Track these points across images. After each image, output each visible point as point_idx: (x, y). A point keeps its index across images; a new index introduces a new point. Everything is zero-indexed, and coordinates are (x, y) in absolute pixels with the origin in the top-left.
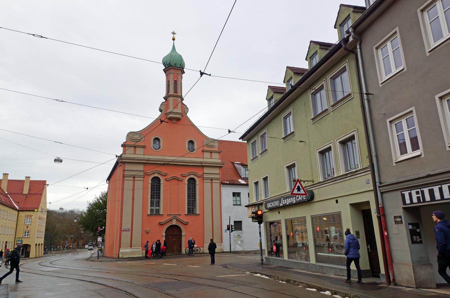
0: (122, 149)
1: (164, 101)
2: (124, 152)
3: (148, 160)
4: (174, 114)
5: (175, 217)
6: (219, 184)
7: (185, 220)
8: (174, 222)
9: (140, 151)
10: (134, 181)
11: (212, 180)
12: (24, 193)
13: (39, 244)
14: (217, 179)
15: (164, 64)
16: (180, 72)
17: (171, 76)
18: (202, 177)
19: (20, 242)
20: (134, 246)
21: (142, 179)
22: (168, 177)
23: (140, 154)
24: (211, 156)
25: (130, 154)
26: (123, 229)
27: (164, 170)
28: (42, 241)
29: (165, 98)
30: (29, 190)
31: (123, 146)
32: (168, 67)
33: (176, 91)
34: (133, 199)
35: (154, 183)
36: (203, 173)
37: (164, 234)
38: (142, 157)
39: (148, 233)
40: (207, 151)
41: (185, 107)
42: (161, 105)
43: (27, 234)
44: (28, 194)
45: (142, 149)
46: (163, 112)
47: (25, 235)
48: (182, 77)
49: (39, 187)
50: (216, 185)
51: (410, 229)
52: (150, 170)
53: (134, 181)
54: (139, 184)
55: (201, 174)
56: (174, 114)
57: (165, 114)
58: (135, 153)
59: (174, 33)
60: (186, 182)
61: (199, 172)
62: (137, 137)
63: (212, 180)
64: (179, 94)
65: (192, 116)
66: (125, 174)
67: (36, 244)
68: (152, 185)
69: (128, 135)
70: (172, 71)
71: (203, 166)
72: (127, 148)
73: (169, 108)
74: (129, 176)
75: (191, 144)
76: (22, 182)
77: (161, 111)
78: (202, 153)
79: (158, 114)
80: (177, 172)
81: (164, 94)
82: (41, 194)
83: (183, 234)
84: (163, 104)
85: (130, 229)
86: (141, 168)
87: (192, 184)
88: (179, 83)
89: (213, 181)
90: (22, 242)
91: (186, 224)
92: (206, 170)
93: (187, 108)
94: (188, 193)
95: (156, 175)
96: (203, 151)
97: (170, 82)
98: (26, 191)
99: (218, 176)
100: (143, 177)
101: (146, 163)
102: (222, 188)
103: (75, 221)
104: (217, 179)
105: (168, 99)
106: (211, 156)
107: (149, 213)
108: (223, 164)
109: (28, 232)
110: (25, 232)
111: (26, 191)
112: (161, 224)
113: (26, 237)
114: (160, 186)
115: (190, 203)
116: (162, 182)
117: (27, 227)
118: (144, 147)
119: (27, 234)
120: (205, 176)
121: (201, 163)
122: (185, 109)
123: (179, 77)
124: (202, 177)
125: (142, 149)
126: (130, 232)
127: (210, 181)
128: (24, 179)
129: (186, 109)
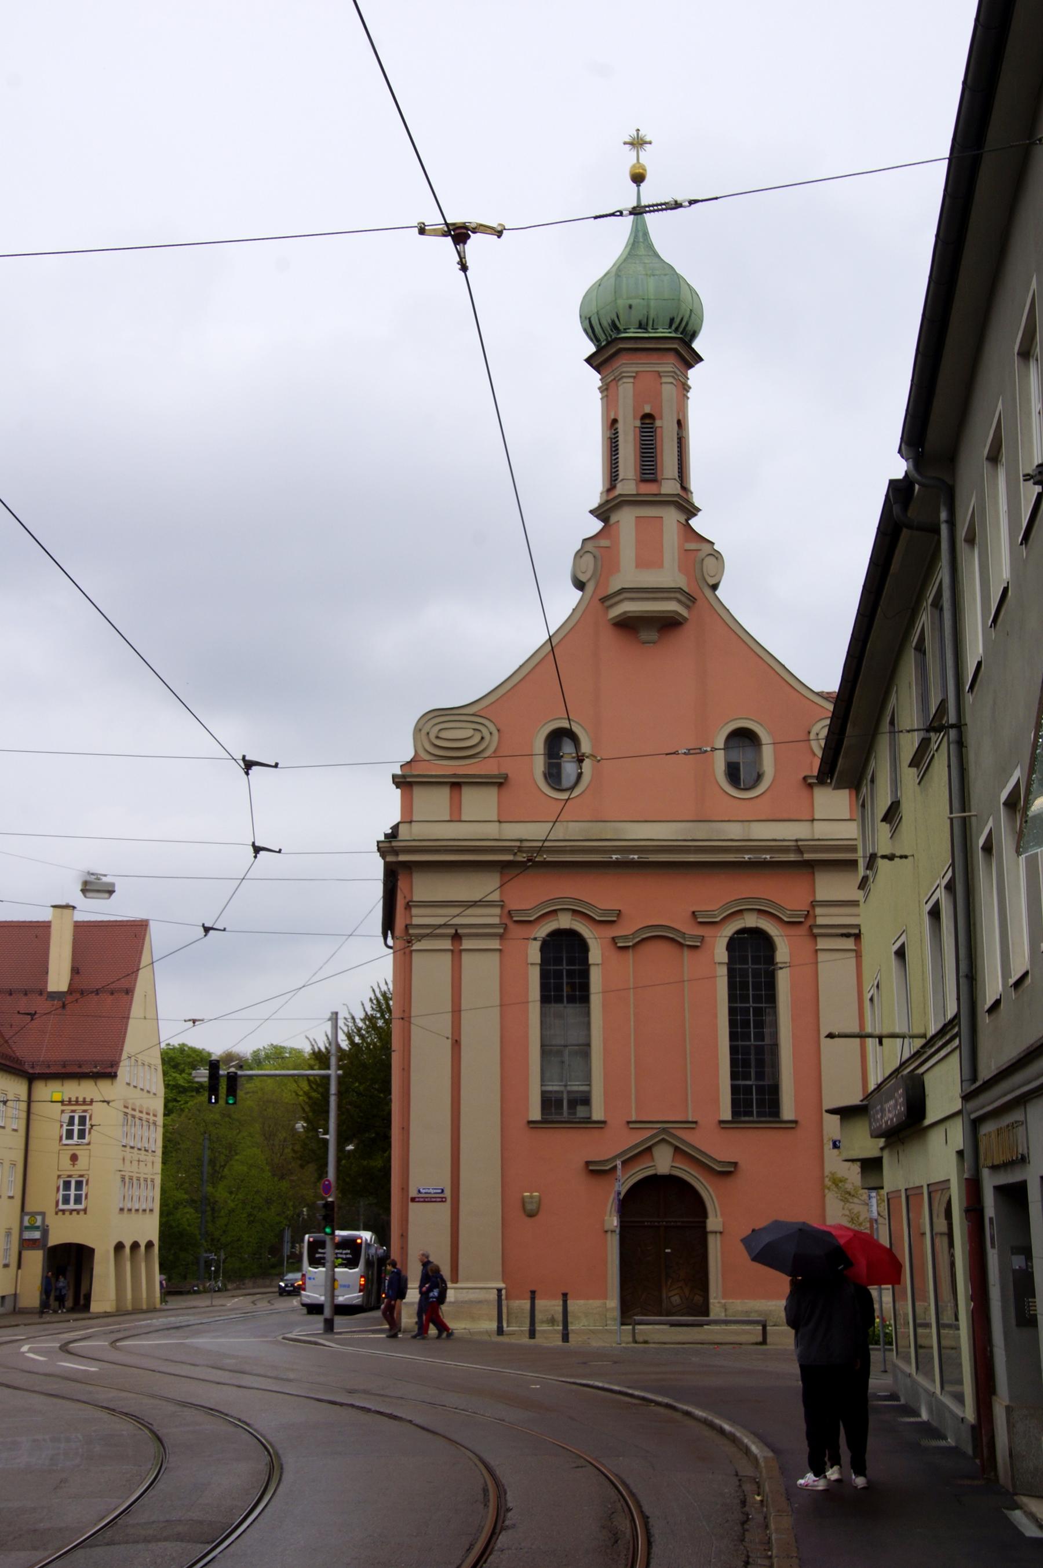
2: (407, 806)
5: (665, 1133)
8: (663, 1163)
9: (480, 804)
10: (457, 954)
12: (52, 987)
13: (135, 1246)
15: (591, 332)
16: (668, 364)
17: (626, 390)
18: (804, 923)
19: (37, 1235)
20: (467, 1280)
21: (495, 944)
23: (480, 819)
25: (438, 822)
27: (601, 894)
28: (148, 1229)
29: (603, 512)
30: (75, 971)
32: (609, 343)
33: (649, 471)
34: (456, 1043)
35: (558, 961)
36: (814, 904)
37: (614, 1222)
38: (491, 830)
39: (531, 1215)
41: (706, 547)
42: (579, 555)
43: (73, 1192)
44: (71, 990)
45: (492, 793)
46: (590, 588)
47: (66, 1200)
48: (686, 388)
49: (114, 955)
51: (1014, 1271)
52: (530, 894)
53: (457, 954)
54: (482, 969)
57: (603, 600)
58: (456, 818)
59: (638, 143)
60: (721, 954)
61: (788, 894)
62: (462, 733)
64: (669, 487)
66: (416, 921)
67: (119, 1247)
68: (544, 975)
69: (418, 730)
70: (627, 365)
71: (811, 867)
72: (418, 792)
73: (618, 570)
74: (432, 932)
76: (44, 928)
77: (580, 585)
78: (804, 792)
79: (565, 601)
80: (670, 904)
81: (594, 493)
82: (129, 992)
83: (713, 1223)
84: (589, 546)
85: (448, 1193)
86: (484, 887)
87: (756, 960)
88: (666, 426)
90: (45, 1232)
91: (727, 1172)
93: (717, 556)
94: (732, 1011)
95: (565, 922)
97: (620, 426)
98: (59, 979)
100: (501, 937)
103: (300, 1126)
105: (613, 519)
107: (536, 1114)
109: (79, 1185)
110: (67, 1185)
111: (59, 979)
112: (597, 1171)
113: (72, 1206)
114: (585, 974)
116: (595, 955)
117: (74, 1158)
118: (500, 783)
119: (73, 1192)
121: (799, 850)
122: (702, 558)
123: (668, 391)
124: (804, 923)
125: (491, 795)
126: (446, 1207)
128: (45, 915)
129: (710, 562)
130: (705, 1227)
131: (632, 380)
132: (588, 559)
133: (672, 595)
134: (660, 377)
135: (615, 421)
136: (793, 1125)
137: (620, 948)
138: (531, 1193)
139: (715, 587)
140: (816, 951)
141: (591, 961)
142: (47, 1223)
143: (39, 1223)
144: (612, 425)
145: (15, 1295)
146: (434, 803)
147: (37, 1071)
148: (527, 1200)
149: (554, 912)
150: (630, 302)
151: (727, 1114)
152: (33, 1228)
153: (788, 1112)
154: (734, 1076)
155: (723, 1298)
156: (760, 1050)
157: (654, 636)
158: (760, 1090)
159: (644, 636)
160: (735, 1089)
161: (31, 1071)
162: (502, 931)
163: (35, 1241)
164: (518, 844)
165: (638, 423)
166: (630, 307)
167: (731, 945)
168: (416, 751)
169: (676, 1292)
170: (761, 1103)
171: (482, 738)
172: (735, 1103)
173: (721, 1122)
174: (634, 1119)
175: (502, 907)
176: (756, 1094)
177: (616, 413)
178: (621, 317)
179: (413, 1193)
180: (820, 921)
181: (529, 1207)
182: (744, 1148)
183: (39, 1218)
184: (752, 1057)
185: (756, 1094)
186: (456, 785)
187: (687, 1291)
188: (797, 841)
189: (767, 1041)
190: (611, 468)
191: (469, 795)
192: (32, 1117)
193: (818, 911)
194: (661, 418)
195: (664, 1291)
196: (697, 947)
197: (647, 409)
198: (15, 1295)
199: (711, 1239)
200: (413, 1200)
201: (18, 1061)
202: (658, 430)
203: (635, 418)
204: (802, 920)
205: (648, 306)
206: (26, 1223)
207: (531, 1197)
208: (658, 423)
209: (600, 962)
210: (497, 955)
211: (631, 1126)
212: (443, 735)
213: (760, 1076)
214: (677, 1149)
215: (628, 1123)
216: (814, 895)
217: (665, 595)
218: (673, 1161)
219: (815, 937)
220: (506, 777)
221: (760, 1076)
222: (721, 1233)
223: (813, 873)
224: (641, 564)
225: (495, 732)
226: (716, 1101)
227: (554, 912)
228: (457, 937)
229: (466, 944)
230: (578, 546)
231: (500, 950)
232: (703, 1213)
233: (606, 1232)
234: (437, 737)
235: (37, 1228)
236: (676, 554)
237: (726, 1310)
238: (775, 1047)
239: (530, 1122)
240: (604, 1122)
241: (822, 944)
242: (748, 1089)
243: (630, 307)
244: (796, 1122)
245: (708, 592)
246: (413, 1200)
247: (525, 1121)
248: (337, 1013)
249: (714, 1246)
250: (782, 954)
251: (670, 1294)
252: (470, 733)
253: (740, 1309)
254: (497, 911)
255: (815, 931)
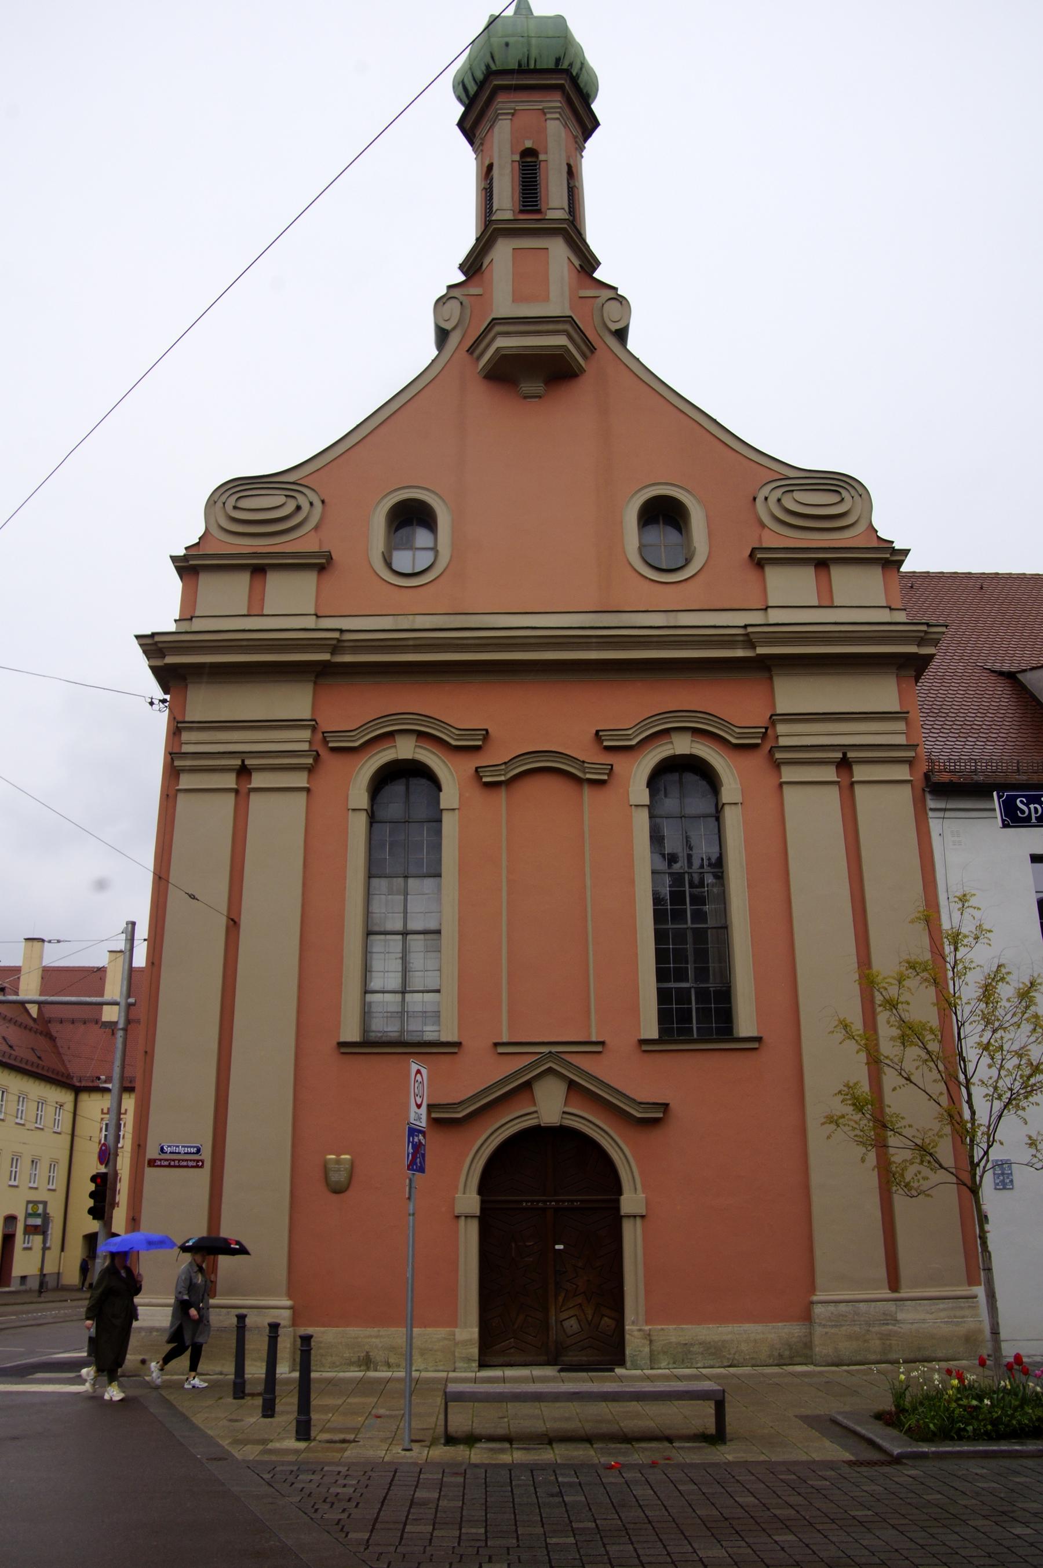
0: (174, 584)
1: (460, 278)
3: (336, 647)
4: (532, 334)
5: (552, 1061)
6: (906, 792)
7: (637, 1080)
8: (550, 1106)
10: (848, 790)
11: (844, 764)
14: (882, 755)
21: (300, 780)
22: (495, 756)
23: (291, 604)
24: (826, 590)
26: (152, 1152)
27: (459, 709)
31: (190, 566)
34: (233, 924)
36: (775, 719)
37: (470, 1201)
39: (338, 1190)
40: (791, 558)
41: (610, 294)
45: (308, 581)
50: (886, 803)
52: (352, 710)
53: (241, 795)
55: (762, 720)
56: (532, 334)
60: (640, 793)
61: (738, 706)
63: (844, 764)
65: (659, 343)
69: (212, 503)
71: (765, 667)
72: (207, 582)
75: (663, 536)
78: (752, 575)
81: (464, 236)
83: (631, 1201)
84: (455, 293)
85: (206, 1155)
86: (295, 702)
89: (860, 773)
91: (652, 1119)
92: (794, 695)
93: (621, 300)
96: (760, 561)
97: (495, 172)
99: (894, 734)
100: (310, 770)
101: (326, 666)
102: (935, 825)
104: (882, 755)
106: (826, 590)
108: (921, 642)
115: (680, 956)
118: (321, 565)
120: (788, 735)
121: (749, 642)
124: (760, 745)
126: (203, 1176)
127: (829, 773)
129: (613, 307)
130: (618, 1209)
131: (510, 117)
132: (454, 306)
133: (560, 327)
134: (545, 114)
135: (490, 167)
136: (755, 1045)
137: (488, 785)
138: (338, 1155)
139: (621, 335)
140: (781, 785)
141: (443, 805)
142: (48, 1211)
143: (40, 1211)
144: (487, 173)
145: (59, 1273)
146: (227, 599)
147: (83, 1084)
148: (331, 1166)
149: (391, 735)
150: (507, 39)
151: (653, 1033)
152: (35, 1215)
153: (745, 1024)
154: (662, 975)
155: (647, 1323)
156: (700, 935)
157: (538, 387)
158: (703, 995)
159: (527, 387)
160: (663, 996)
161: (78, 1084)
162: (310, 761)
163: (36, 1227)
164: (336, 635)
165: (517, 158)
166: (507, 44)
167: (654, 780)
168: (206, 528)
169: (572, 1312)
170: (704, 1014)
171: (299, 508)
172: (664, 1016)
173: (643, 1042)
174: (505, 1040)
175: (314, 729)
176: (696, 1005)
177: (491, 157)
178: (496, 58)
179: (152, 1152)
180: (783, 742)
181: (334, 1177)
182: (682, 1081)
183: (41, 1206)
184: (689, 947)
185: (696, 1005)
186: (259, 571)
187: (590, 1312)
188: (745, 627)
189: (711, 923)
190: (486, 217)
191: (275, 581)
192: (78, 1118)
193: (781, 728)
194: (546, 153)
195: (552, 1312)
196: (602, 783)
197: (528, 144)
198: (59, 1273)
199: (627, 1227)
200: (152, 1163)
201: (69, 1076)
202: (542, 164)
203: (512, 153)
204: (759, 741)
205: (529, 44)
206: (30, 1211)
207: (338, 1162)
208: (542, 157)
209: (456, 806)
210: (303, 796)
211: (501, 1050)
212: (243, 504)
213: (702, 973)
214: (572, 1085)
215: (496, 1045)
216: (773, 705)
217: (551, 327)
218: (565, 1105)
219: (777, 765)
220: (329, 557)
221: (702, 973)
222: (642, 1217)
223: (771, 678)
224: (518, 298)
225: (318, 503)
226: (635, 1010)
227: (391, 735)
228: (244, 772)
229: (258, 780)
230: (444, 291)
231: (308, 790)
232: (617, 1188)
233: (458, 1217)
234: (235, 508)
235: (39, 1215)
236: (566, 289)
237: (651, 1341)
238: (724, 928)
239: (342, 1045)
240: (458, 1044)
241: (789, 774)
242: (683, 996)
243: (507, 44)
244: (758, 1039)
245: (612, 342)
246: (152, 1163)
247: (335, 1043)
248: (133, 924)
249: (632, 1236)
250: (731, 789)
251: (564, 1316)
252: (282, 500)
253: (673, 1339)
254: (306, 734)
255: (778, 755)
